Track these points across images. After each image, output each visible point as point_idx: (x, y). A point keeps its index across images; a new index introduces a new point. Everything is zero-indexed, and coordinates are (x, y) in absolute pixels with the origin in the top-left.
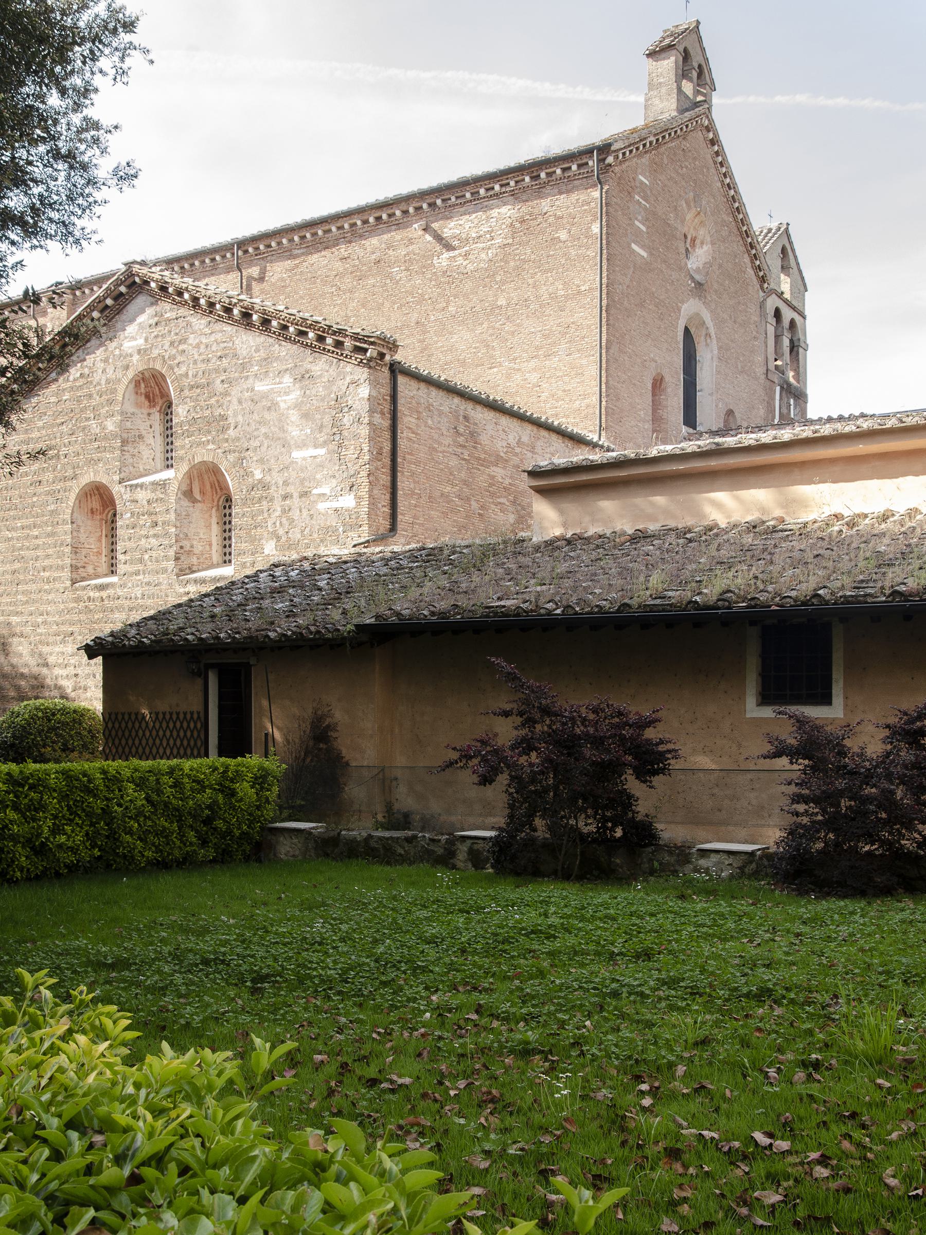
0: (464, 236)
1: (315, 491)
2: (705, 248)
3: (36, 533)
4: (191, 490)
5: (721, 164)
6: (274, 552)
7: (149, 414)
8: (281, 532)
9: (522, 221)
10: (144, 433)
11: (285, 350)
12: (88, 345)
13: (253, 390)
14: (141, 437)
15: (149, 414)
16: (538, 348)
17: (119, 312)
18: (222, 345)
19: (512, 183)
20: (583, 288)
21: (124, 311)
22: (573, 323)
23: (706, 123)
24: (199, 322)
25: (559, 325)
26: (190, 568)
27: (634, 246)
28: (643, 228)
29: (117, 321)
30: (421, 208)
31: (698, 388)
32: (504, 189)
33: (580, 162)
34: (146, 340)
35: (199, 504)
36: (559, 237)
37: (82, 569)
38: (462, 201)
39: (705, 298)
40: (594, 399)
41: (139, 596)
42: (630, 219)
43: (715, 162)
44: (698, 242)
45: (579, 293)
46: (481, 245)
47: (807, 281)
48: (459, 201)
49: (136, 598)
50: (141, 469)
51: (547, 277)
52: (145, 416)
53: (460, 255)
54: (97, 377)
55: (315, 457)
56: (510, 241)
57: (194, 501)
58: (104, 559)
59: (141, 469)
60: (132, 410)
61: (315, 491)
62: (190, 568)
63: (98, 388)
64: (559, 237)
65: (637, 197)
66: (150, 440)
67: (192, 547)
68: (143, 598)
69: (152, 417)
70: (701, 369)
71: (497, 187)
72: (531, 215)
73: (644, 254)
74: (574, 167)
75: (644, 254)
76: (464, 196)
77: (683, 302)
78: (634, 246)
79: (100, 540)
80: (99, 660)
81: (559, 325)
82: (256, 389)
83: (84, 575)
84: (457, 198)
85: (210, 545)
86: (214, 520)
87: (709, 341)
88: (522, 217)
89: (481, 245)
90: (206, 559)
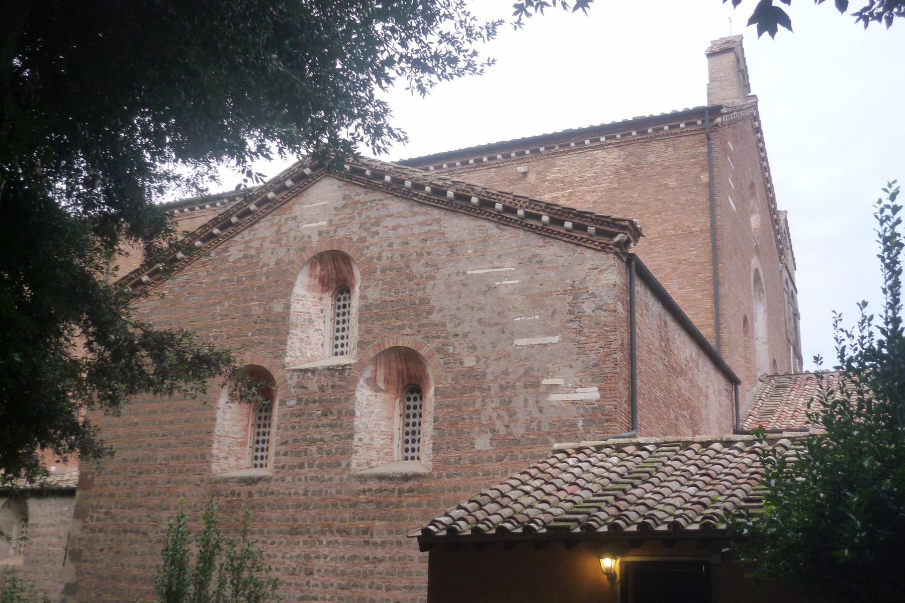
0: (567, 180)
1: (545, 382)
3: (171, 418)
4: (375, 378)
6: (489, 447)
7: (321, 299)
8: (499, 425)
10: (314, 316)
11: (512, 238)
12: (256, 226)
13: (465, 273)
14: (311, 321)
15: (321, 299)
17: (298, 194)
18: (426, 228)
19: (618, 136)
21: (305, 194)
24: (397, 206)
25: (669, 261)
26: (368, 463)
29: (294, 204)
30: (524, 153)
32: (609, 142)
34: (330, 221)
35: (382, 394)
37: (224, 461)
38: (566, 149)
40: (710, 329)
41: (302, 492)
46: (586, 188)
47: (796, 261)
48: (562, 150)
49: (296, 493)
50: (309, 355)
51: (655, 218)
52: (316, 300)
53: (563, 196)
54: (264, 257)
55: (545, 345)
56: (616, 185)
57: (377, 390)
58: (248, 450)
59: (309, 355)
60: (303, 293)
61: (545, 382)
62: (368, 463)
63: (265, 269)
64: (667, 184)
66: (318, 323)
67: (372, 439)
68: (305, 495)
69: (324, 302)
71: (603, 139)
72: (637, 164)
73: (734, 208)
75: (734, 208)
76: (569, 145)
79: (246, 430)
80: (427, 553)
82: (469, 272)
83: (226, 466)
84: (561, 147)
85: (392, 439)
86: (397, 412)
87: (762, 295)
89: (586, 188)
90: (387, 454)
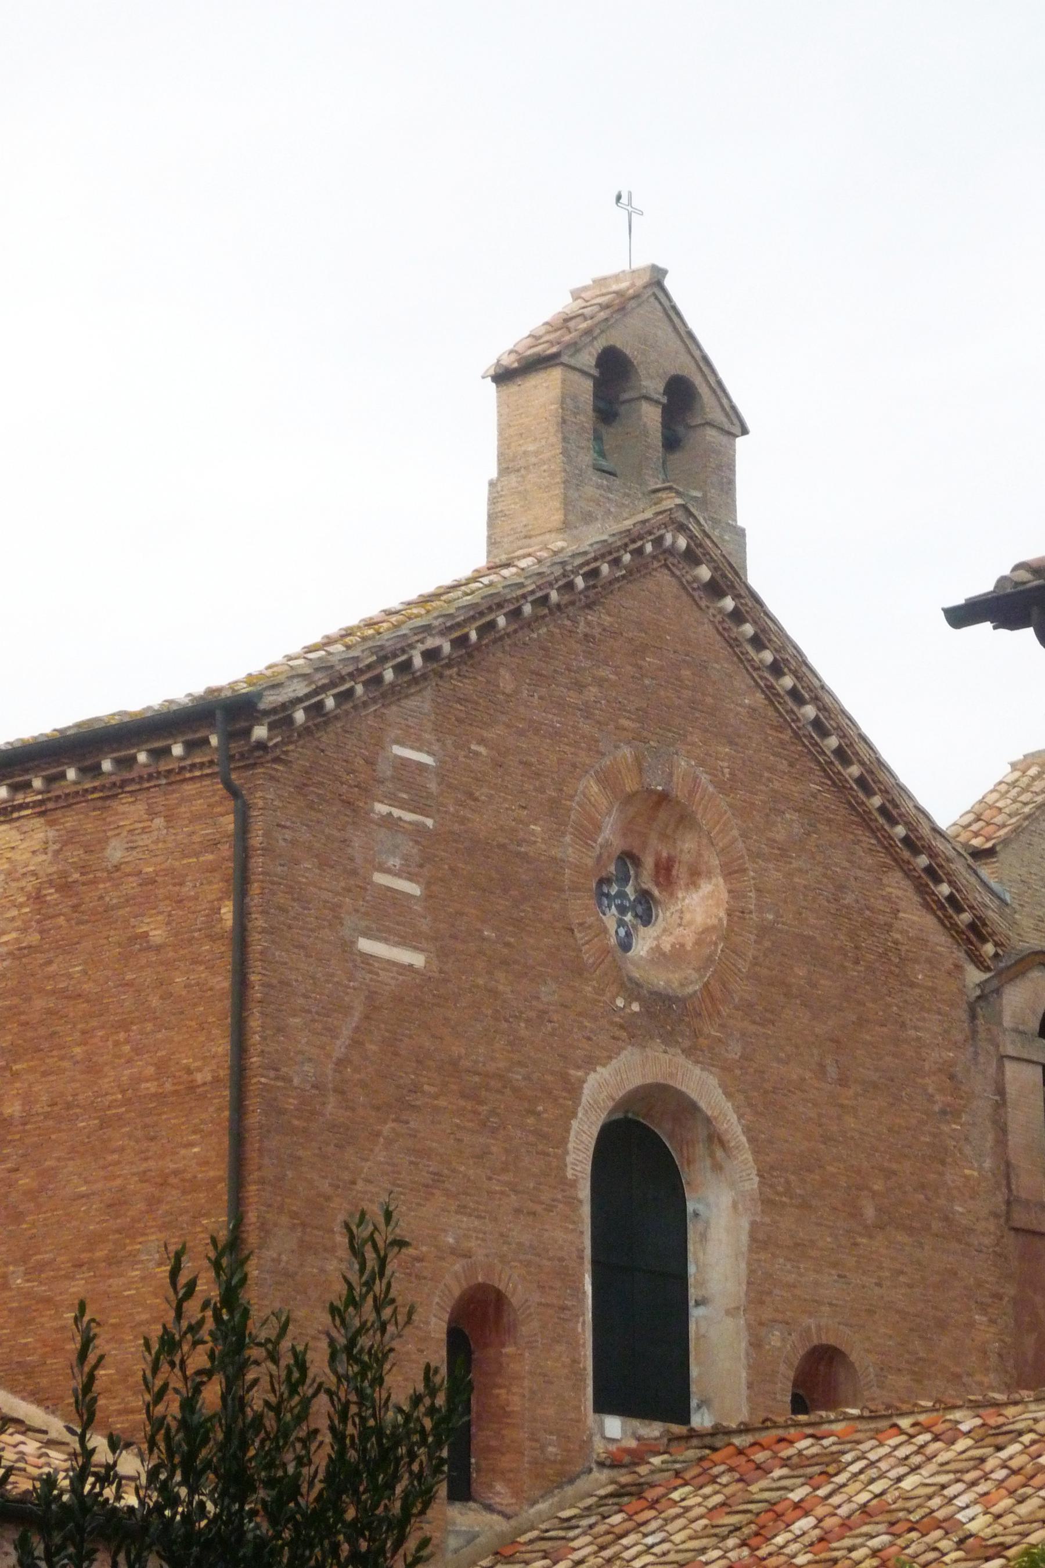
2: (706, 887)
5: (758, 642)
9: (65, 887)
16: (94, 1241)
19: (37, 783)
20: (199, 1077)
22: (176, 1173)
23: (682, 543)
27: (365, 945)
28: (413, 889)
31: (693, 1293)
33: (190, 737)
36: (145, 935)
39: (696, 1034)
42: (354, 873)
43: (733, 643)
44: (680, 872)
45: (192, 1088)
56: (34, 938)
64: (145, 935)
65: (381, 808)
70: (703, 1237)
72: (84, 869)
74: (177, 750)
77: (590, 1063)
78: (365, 945)
81: (144, 1177)
87: (719, 1154)
88: (63, 874)
